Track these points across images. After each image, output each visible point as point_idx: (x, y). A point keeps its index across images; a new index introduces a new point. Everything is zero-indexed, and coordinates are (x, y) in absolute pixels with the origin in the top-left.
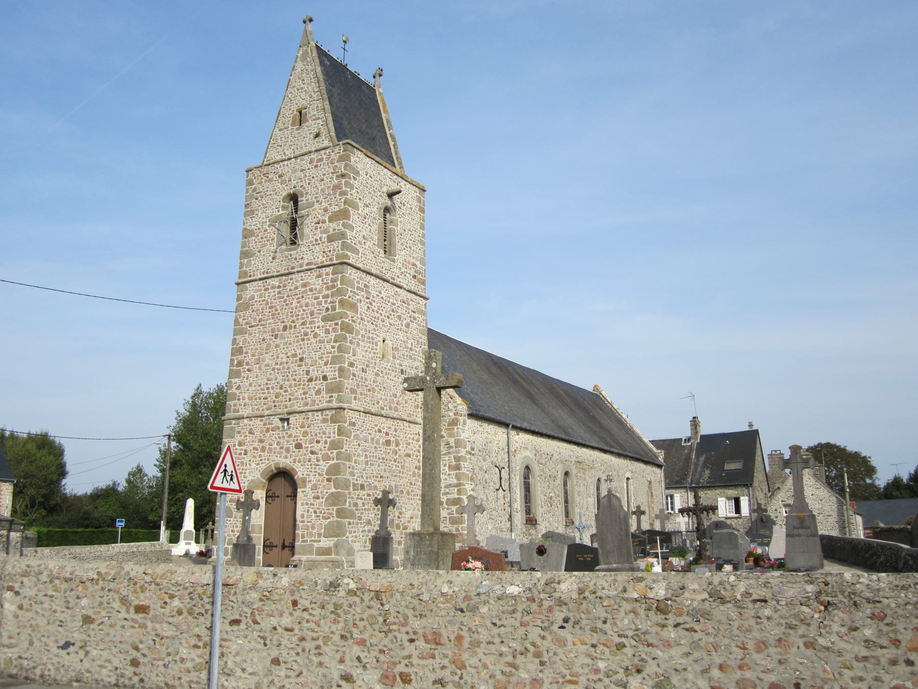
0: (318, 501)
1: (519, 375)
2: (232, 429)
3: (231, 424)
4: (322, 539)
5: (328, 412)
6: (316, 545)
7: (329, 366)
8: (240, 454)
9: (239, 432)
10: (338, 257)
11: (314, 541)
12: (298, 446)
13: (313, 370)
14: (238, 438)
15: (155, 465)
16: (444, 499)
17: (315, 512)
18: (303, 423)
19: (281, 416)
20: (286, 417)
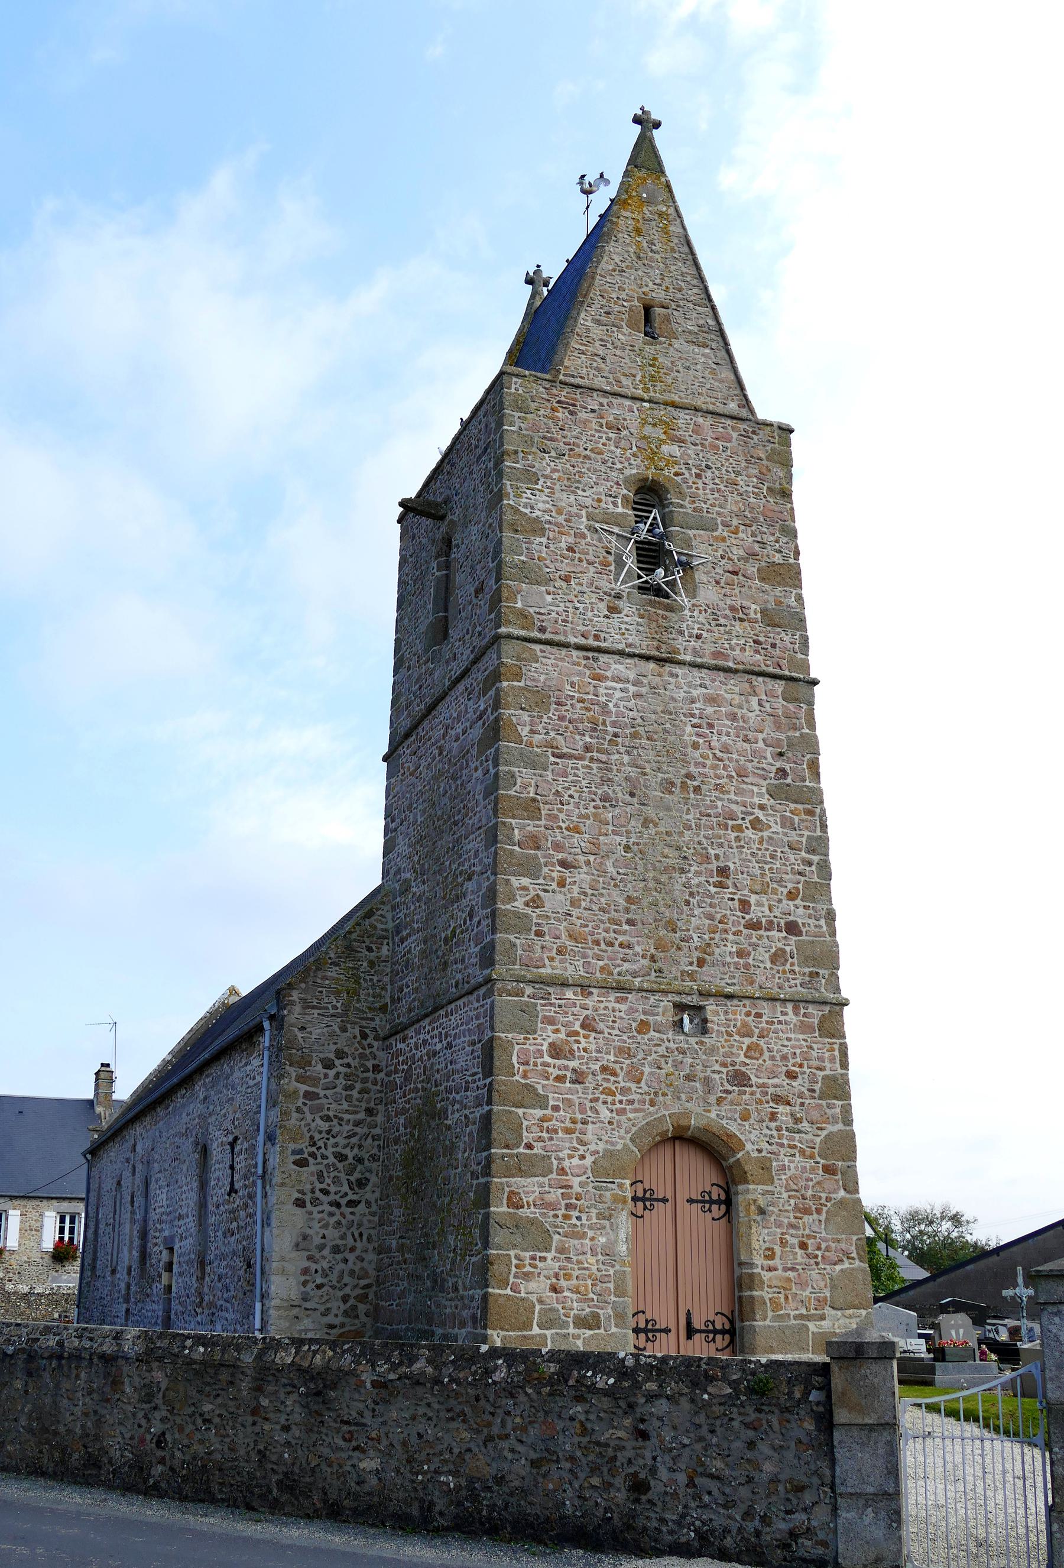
0: (806, 1218)
1: (263, 1245)
2: (529, 1011)
3: (520, 993)
4: (828, 1311)
5: (811, 1009)
6: (812, 1326)
7: (798, 902)
8: (560, 1079)
9: (551, 1021)
10: (546, 997)
11: (808, 1318)
12: (740, 1079)
13: (759, 904)
14: (547, 1036)
15: (104, 1076)
16: (191, 1218)
17: (803, 1246)
18: (745, 1024)
19: (677, 998)
20: (694, 1000)
